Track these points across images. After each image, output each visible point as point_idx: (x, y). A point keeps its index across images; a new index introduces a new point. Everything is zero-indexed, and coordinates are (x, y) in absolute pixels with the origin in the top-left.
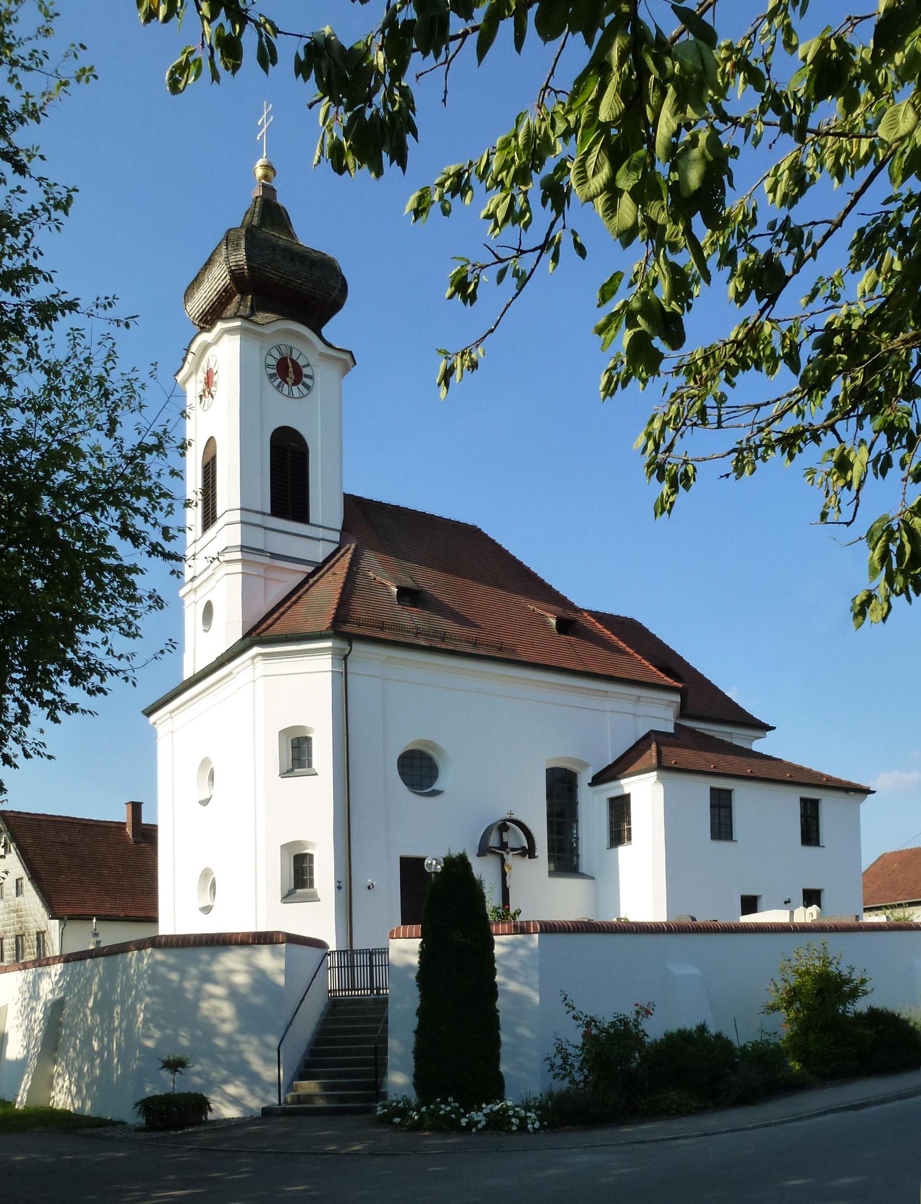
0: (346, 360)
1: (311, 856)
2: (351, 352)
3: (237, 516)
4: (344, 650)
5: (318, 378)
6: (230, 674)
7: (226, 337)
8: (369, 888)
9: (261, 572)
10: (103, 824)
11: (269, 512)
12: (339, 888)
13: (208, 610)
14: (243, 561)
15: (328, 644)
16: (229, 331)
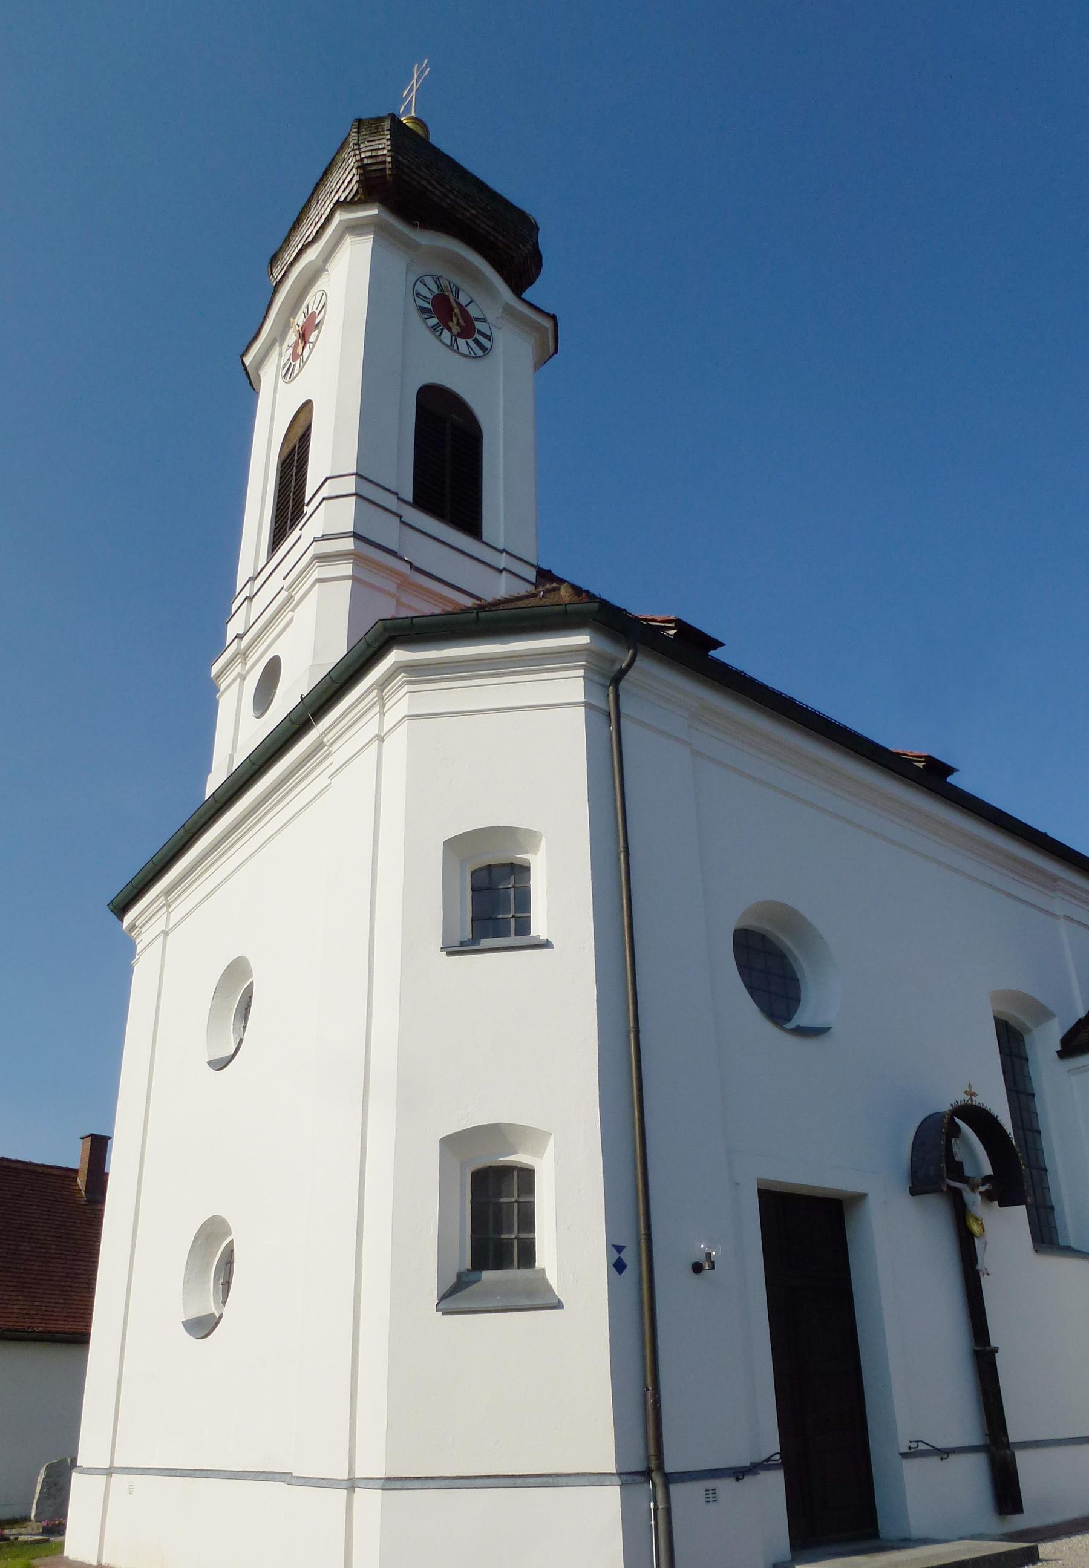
0: (546, 329)
1: (527, 1175)
2: (553, 318)
3: (349, 485)
4: (613, 661)
5: (497, 335)
6: (319, 746)
7: (349, 241)
8: (697, 1268)
9: (391, 586)
10: (40, 1170)
11: (411, 501)
12: (619, 1266)
13: (236, 993)
14: (354, 556)
15: (582, 639)
16: (355, 228)
